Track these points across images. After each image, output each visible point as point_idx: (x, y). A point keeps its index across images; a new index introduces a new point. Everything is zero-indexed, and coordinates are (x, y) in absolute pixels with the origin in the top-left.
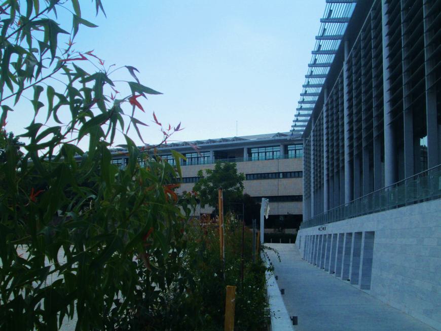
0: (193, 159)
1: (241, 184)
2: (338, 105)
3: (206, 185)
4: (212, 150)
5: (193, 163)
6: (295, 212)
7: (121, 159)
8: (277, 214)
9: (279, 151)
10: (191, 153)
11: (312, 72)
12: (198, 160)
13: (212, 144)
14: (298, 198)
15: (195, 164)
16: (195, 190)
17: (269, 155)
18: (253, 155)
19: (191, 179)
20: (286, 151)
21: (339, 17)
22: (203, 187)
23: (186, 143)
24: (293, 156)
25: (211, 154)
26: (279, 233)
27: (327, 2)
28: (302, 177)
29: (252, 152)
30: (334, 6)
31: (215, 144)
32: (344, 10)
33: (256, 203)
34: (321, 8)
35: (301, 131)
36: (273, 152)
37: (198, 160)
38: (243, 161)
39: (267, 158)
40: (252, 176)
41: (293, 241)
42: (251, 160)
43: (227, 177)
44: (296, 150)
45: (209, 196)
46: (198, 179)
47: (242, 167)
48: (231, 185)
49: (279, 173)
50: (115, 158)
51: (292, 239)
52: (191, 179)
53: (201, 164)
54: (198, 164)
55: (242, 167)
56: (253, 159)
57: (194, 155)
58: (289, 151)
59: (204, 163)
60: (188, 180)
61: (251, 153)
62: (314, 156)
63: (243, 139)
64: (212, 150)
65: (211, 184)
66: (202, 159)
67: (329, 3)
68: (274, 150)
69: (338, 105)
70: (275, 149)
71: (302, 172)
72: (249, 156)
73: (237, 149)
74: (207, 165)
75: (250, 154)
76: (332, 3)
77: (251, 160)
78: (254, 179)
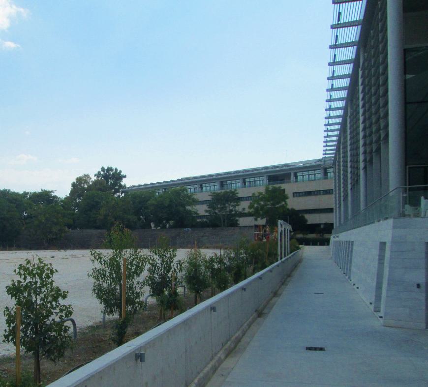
0: (251, 183)
1: (285, 202)
2: (378, 130)
3: (258, 203)
4: (265, 175)
5: (251, 185)
6: (329, 222)
7: (239, 179)
8: (318, 223)
9: (320, 174)
10: (309, 171)
11: (331, 96)
12: (309, 177)
13: (266, 170)
14: (330, 210)
15: (253, 186)
16: (250, 207)
17: (312, 177)
18: (299, 177)
19: (245, 198)
20: (326, 173)
21: (358, 19)
22: (256, 206)
23: (210, 176)
24: (301, 180)
25: (265, 178)
26: (321, 237)
27: (334, 3)
28: (333, 193)
29: (298, 175)
30: (344, 7)
31: (268, 170)
32: (355, 11)
33: (300, 215)
34: (328, 12)
35: (332, 157)
36: (303, 176)
37: (309, 177)
38: (290, 182)
39: (310, 179)
40: (298, 194)
41: (328, 244)
42: (327, 178)
43: (278, 196)
44: (303, 176)
45: (261, 212)
46: (254, 198)
47: (288, 188)
48: (278, 203)
49: (320, 191)
50: (306, 170)
51: (326, 242)
52: (245, 198)
53: (257, 186)
54: (255, 186)
55: (288, 188)
56: (299, 180)
57: (252, 179)
58: (329, 173)
59: (260, 185)
60: (246, 199)
61: (327, 173)
62: (352, 174)
63: (189, 179)
64: (265, 175)
65: (262, 203)
66: (258, 182)
67: (337, 3)
68: (316, 173)
69: (378, 130)
70: (317, 172)
71: (332, 190)
72: (295, 178)
73: (287, 173)
74: (261, 187)
75: (296, 177)
76: (340, 3)
77: (327, 178)
78: (299, 196)
